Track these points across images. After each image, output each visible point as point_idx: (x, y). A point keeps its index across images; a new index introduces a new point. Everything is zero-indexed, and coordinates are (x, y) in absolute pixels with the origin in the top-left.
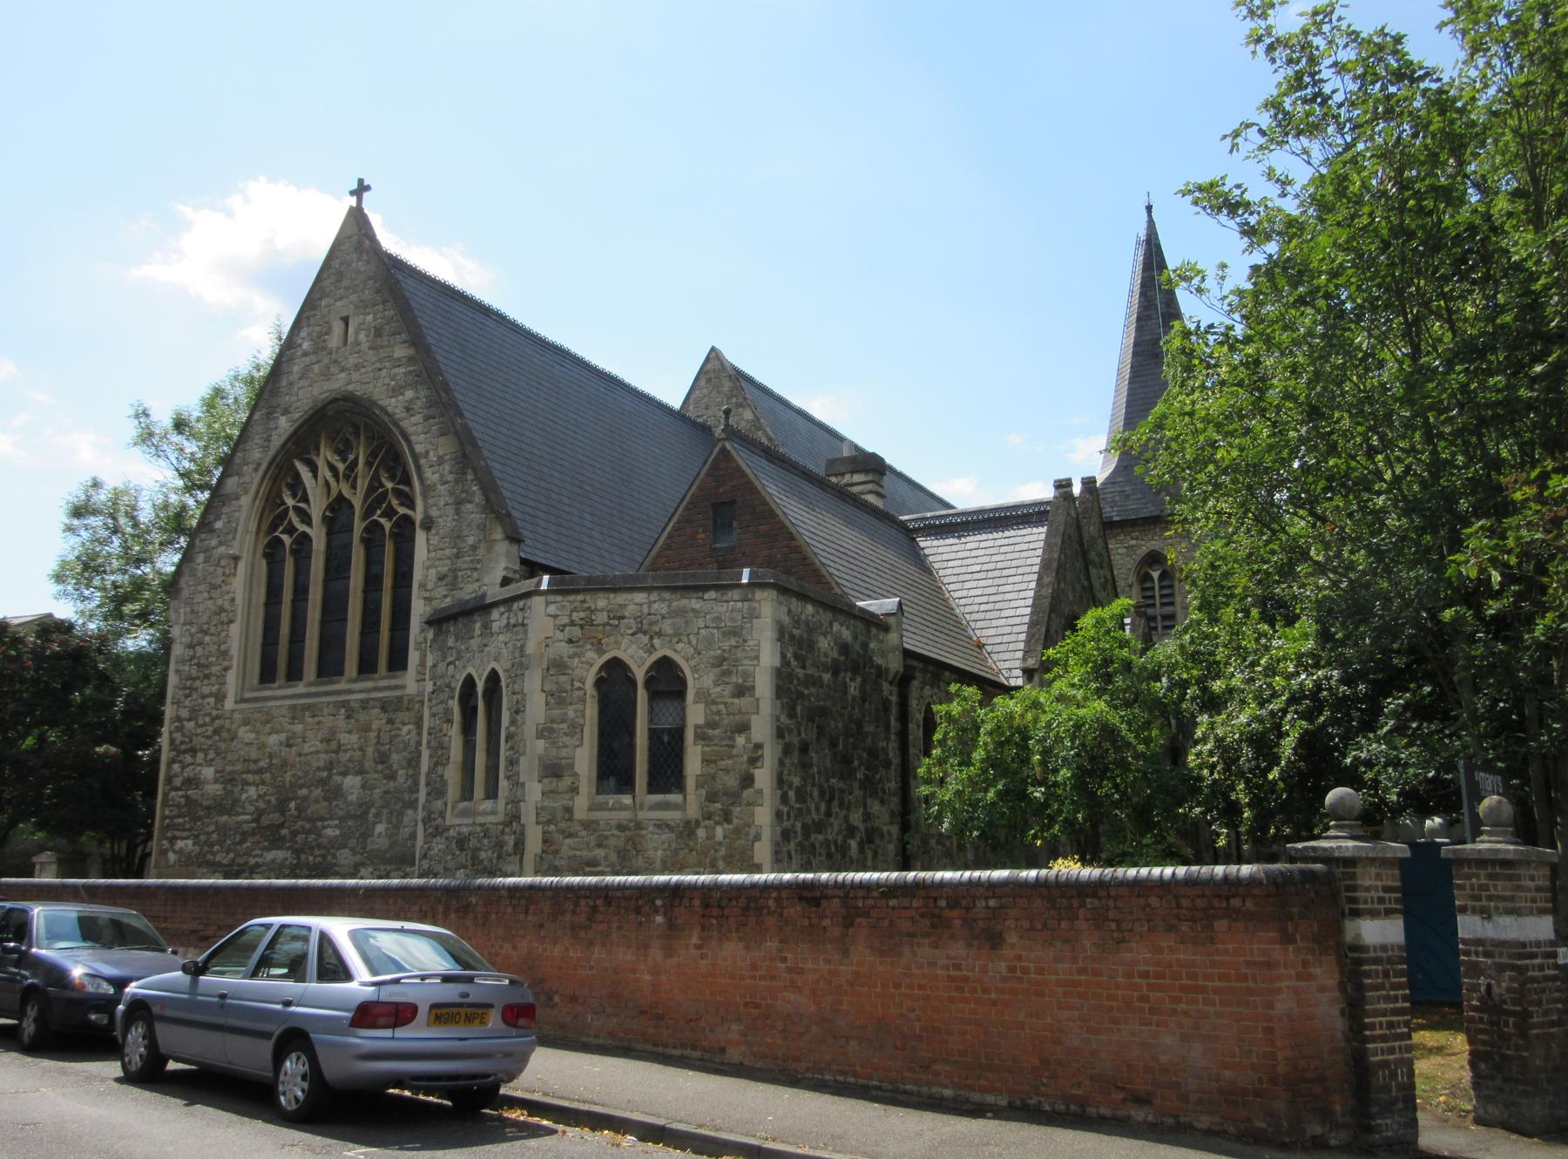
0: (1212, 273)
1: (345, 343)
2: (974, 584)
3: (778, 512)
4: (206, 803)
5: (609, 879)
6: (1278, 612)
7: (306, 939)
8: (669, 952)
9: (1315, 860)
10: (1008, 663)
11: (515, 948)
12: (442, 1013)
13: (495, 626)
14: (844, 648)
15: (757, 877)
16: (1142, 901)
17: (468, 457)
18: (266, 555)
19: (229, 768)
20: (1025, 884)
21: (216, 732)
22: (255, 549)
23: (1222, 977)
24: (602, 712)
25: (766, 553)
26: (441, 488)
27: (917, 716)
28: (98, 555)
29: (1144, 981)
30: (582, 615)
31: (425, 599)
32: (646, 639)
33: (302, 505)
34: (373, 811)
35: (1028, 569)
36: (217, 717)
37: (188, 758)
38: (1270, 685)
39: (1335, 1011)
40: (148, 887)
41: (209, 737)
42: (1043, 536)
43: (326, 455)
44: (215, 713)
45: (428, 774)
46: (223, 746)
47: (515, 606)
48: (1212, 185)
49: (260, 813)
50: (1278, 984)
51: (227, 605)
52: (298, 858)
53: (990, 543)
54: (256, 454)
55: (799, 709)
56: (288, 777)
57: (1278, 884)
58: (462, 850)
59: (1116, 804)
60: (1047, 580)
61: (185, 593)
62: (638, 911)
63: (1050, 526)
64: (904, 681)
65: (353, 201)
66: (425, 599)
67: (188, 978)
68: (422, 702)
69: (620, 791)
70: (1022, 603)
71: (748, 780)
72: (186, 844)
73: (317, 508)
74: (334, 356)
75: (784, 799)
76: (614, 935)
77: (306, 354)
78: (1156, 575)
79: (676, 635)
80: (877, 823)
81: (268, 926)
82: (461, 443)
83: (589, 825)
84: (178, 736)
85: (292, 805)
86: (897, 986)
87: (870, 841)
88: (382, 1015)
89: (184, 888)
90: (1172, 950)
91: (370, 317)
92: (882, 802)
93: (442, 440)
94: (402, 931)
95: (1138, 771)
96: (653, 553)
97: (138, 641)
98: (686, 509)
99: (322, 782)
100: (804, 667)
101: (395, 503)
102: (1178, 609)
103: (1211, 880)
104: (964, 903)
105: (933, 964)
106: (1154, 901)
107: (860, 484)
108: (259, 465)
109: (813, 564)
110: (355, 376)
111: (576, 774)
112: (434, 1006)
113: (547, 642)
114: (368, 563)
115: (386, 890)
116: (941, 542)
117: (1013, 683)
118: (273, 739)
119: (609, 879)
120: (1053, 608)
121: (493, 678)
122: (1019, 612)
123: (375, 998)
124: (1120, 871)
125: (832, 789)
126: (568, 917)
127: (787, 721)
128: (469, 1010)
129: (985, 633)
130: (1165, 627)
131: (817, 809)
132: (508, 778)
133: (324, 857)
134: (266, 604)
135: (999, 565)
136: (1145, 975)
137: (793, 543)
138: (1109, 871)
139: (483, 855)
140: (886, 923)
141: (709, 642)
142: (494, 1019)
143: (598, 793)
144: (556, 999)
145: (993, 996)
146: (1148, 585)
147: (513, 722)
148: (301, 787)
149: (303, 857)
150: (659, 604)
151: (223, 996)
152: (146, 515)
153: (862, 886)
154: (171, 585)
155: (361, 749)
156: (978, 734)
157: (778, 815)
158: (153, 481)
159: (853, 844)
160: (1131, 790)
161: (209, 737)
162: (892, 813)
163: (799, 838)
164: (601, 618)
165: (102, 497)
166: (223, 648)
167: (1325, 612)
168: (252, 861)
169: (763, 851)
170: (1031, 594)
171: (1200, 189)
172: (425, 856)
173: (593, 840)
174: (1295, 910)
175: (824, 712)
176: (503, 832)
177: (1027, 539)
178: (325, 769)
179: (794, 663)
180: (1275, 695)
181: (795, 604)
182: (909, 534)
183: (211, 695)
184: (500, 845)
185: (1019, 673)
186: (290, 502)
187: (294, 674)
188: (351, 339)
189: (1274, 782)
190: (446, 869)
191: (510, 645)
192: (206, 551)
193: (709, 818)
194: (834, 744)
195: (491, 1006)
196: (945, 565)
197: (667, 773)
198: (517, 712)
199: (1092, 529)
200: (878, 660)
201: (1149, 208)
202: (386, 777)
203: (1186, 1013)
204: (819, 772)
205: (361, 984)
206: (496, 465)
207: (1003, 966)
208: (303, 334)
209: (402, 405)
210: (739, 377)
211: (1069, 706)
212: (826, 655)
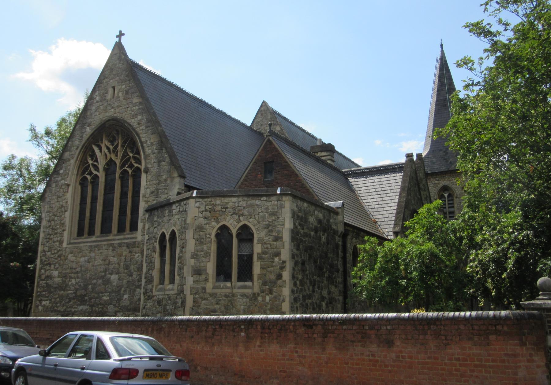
0: (476, 61)
1: (114, 97)
3: (292, 166)
4: (54, 286)
5: (221, 317)
6: (504, 207)
7: (92, 341)
8: (247, 348)
9: (533, 309)
10: (387, 229)
11: (181, 346)
12: (149, 373)
13: (174, 212)
14: (320, 222)
15: (285, 316)
16: (456, 327)
17: (163, 142)
18: (80, 184)
19: (64, 272)
20: (404, 319)
21: (59, 256)
22: (76, 181)
23: (493, 361)
24: (218, 248)
25: (286, 182)
26: (152, 156)
27: (350, 251)
28: (14, 185)
29: (458, 362)
30: (210, 207)
31: (145, 201)
32: (237, 217)
33: (95, 163)
34: (123, 289)
35: (395, 191)
37: (48, 268)
38: (502, 238)
39: (544, 377)
40: (30, 320)
41: (56, 259)
42: (401, 177)
43: (105, 143)
44: (59, 249)
45: (146, 273)
46: (62, 262)
47: (182, 203)
48: (478, 23)
49: (77, 290)
50: (518, 364)
51: (64, 204)
54: (77, 142)
55: (301, 247)
57: (518, 319)
59: (436, 287)
60: (403, 195)
61: (47, 200)
62: (234, 331)
63: (404, 173)
64: (344, 236)
65: (117, 40)
66: (145, 201)
67: (41, 357)
68: (143, 244)
69: (225, 281)
70: (393, 204)
71: (280, 276)
72: (46, 303)
73: (101, 164)
75: (295, 284)
76: (223, 341)
77: (97, 102)
78: (446, 195)
79: (249, 215)
81: (77, 335)
82: (160, 137)
83: (212, 295)
84: (44, 258)
85: (90, 287)
87: (331, 303)
88: (122, 374)
89: (44, 321)
90: (470, 348)
91: (124, 86)
92: (336, 287)
93: (153, 136)
94: (132, 338)
95: (446, 273)
96: (240, 183)
97: (28, 221)
98: (253, 165)
99: (102, 277)
100: (303, 229)
101: (133, 162)
102: (456, 209)
103: (488, 318)
104: (376, 327)
105: (362, 354)
106: (462, 327)
107: (323, 155)
108: (78, 147)
109: (306, 187)
110: (117, 110)
111: (207, 274)
112: (146, 370)
115: (127, 322)
116: (359, 180)
117: (389, 238)
118: (82, 259)
119: (221, 317)
120: (406, 207)
121: (173, 233)
122: (392, 208)
123: (120, 366)
124: (446, 314)
125: (315, 280)
126: (204, 333)
127: (296, 252)
128: (161, 372)
129: (378, 217)
130: (450, 217)
131: (309, 289)
132: (179, 275)
133: (102, 308)
135: (383, 189)
136: (458, 359)
137: (298, 179)
138: (441, 313)
139: (168, 307)
140: (342, 336)
141: (264, 218)
142: (172, 377)
143: (217, 281)
144: (199, 368)
145: (390, 368)
147: (181, 252)
148: (94, 279)
149: (94, 308)
151: (56, 365)
152: (33, 169)
153: (331, 320)
154: (42, 197)
155: (118, 264)
156: (377, 257)
157: (292, 291)
158: (37, 155)
159: (324, 304)
160: (441, 281)
161: (56, 259)
162: (340, 291)
163: (301, 301)
164: (218, 208)
165: (16, 162)
166: (62, 222)
167: (525, 206)
168: (73, 310)
169: (286, 306)
170: (397, 201)
171: (472, 25)
172: (144, 308)
173: (214, 301)
174: (526, 331)
175: (311, 248)
176: (176, 298)
177: (395, 178)
179: (299, 227)
180: (504, 242)
181: (300, 203)
182: (346, 176)
183: (57, 241)
184: (175, 303)
185: (392, 233)
186: (90, 162)
187: (91, 233)
189: (504, 279)
190: (153, 313)
191: (180, 219)
194: (315, 262)
195: (170, 371)
196: (360, 189)
197: (246, 273)
198: (183, 248)
199: (421, 175)
200: (334, 227)
201: (442, 46)
202: (128, 275)
203: (477, 377)
204: (309, 273)
205: (114, 360)
206: (175, 147)
208: (97, 94)
209: (137, 122)
210: (275, 114)
211: (417, 244)
212: (312, 224)
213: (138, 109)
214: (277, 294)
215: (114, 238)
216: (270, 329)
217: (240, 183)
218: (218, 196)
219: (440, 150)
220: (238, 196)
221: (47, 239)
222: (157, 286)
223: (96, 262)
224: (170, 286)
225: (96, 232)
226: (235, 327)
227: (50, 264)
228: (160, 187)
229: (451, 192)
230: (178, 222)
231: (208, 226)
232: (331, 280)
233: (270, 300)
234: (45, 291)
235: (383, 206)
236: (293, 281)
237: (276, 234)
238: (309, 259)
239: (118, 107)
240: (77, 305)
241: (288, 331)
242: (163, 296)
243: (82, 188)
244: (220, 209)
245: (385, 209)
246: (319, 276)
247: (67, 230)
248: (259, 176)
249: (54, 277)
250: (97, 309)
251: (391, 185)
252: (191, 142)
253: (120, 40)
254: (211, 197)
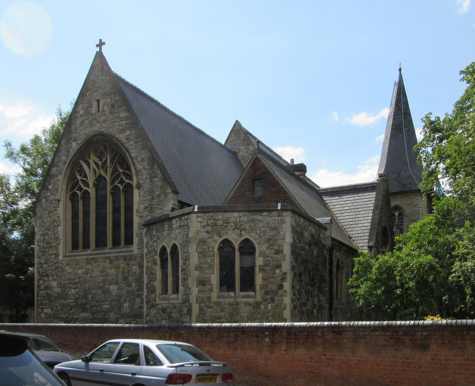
2: (346, 214)
3: (280, 183)
4: (54, 295)
12: (201, 377)
13: (174, 226)
17: (154, 160)
19: (63, 282)
21: (56, 268)
22: (66, 197)
30: (212, 221)
31: (139, 216)
32: (238, 231)
34: (123, 298)
36: (56, 263)
42: (374, 196)
43: (93, 159)
44: (55, 261)
45: (147, 284)
46: (59, 274)
47: (183, 218)
49: (77, 299)
51: (56, 219)
52: (94, 316)
53: (352, 199)
54: (64, 158)
55: (299, 259)
56: (87, 286)
58: (164, 313)
60: (377, 212)
61: (39, 214)
62: (257, 336)
65: (98, 49)
66: (139, 216)
67: (83, 363)
69: (228, 290)
73: (91, 180)
74: (94, 117)
75: (294, 294)
78: (397, 214)
79: (251, 230)
80: (322, 303)
81: (119, 343)
82: (151, 152)
83: (217, 304)
84: (41, 270)
85: (90, 296)
86: (378, 365)
91: (109, 100)
92: (324, 295)
93: (143, 152)
98: (241, 182)
99: (101, 288)
100: (300, 243)
101: (124, 178)
104: (411, 333)
108: (65, 162)
110: (104, 125)
111: (212, 284)
112: (198, 375)
113: (198, 232)
114: (114, 202)
116: (332, 198)
118: (80, 271)
119: (243, 324)
121: (174, 247)
123: (175, 372)
126: (225, 339)
127: (295, 264)
128: (211, 376)
129: (351, 233)
131: (304, 297)
132: (183, 286)
134: (72, 219)
135: (356, 207)
137: (287, 196)
139: (173, 315)
141: (265, 232)
142: (219, 380)
143: (220, 291)
145: (424, 369)
146: (394, 218)
147: (184, 264)
148: (93, 289)
149: (96, 315)
150: (244, 217)
151: (102, 371)
155: (116, 275)
157: (292, 300)
163: (299, 309)
164: (220, 223)
166: (56, 236)
168: (75, 317)
169: (287, 313)
170: (371, 218)
175: (306, 261)
177: (367, 197)
178: (102, 282)
179: (297, 241)
181: (297, 218)
183: (53, 254)
184: (181, 311)
186: (79, 178)
187: (86, 246)
188: (101, 109)
191: (181, 234)
192: (46, 198)
193: (265, 301)
196: (334, 207)
197: (248, 283)
198: (186, 260)
201: (400, 70)
202: (127, 286)
204: (305, 284)
207: (429, 358)
208: (80, 107)
210: (247, 133)
212: (307, 239)
213: (126, 124)
214: (278, 302)
215: (110, 251)
216: (296, 335)
217: (228, 199)
218: (219, 211)
219: (394, 172)
220: (239, 211)
221: (42, 252)
222: (160, 295)
223: (94, 274)
224: (174, 296)
225: (91, 245)
226: (258, 333)
227: (48, 276)
228: (153, 202)
229: (401, 212)
230: (179, 236)
231: (210, 240)
232: (320, 289)
233: (272, 308)
234: (46, 300)
235: (356, 223)
236: (292, 291)
237: (277, 248)
238: (304, 271)
239: (104, 121)
240: (79, 312)
241: (316, 337)
242: (167, 305)
243: (72, 203)
244: (222, 223)
245: (359, 225)
246: (312, 286)
247: (62, 243)
248: (247, 193)
249: (53, 288)
250: (99, 316)
251: (363, 203)
252: (177, 158)
253: (101, 49)
254: (213, 212)
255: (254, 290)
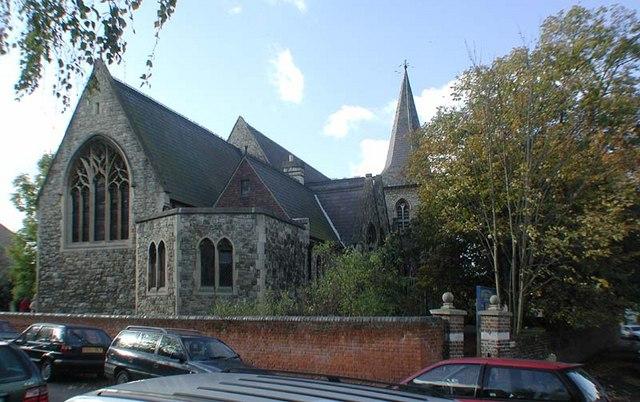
1: (98, 113)
43: (92, 157)
69: (209, 285)
71: (254, 283)
73: (91, 177)
78: (403, 207)
114: (112, 199)
186: (80, 174)
187: (85, 239)
197: (226, 280)
227: (49, 266)
255: (231, 284)
